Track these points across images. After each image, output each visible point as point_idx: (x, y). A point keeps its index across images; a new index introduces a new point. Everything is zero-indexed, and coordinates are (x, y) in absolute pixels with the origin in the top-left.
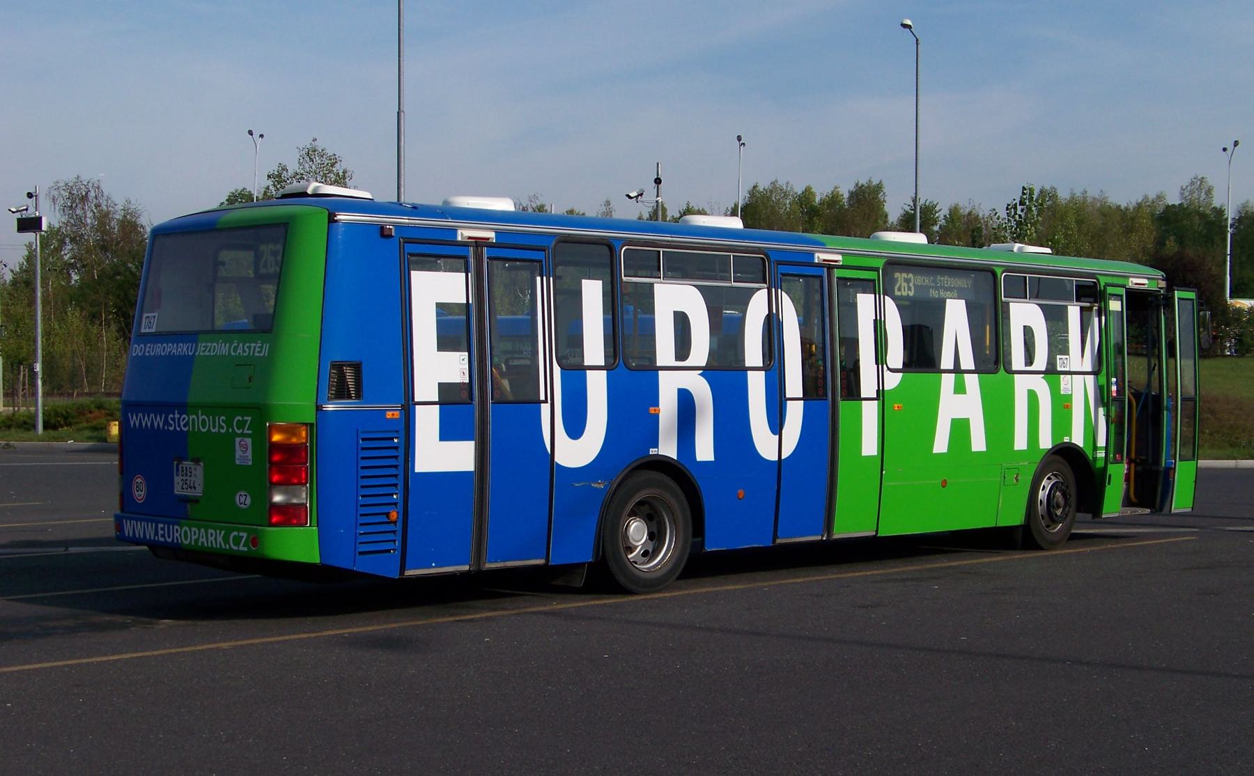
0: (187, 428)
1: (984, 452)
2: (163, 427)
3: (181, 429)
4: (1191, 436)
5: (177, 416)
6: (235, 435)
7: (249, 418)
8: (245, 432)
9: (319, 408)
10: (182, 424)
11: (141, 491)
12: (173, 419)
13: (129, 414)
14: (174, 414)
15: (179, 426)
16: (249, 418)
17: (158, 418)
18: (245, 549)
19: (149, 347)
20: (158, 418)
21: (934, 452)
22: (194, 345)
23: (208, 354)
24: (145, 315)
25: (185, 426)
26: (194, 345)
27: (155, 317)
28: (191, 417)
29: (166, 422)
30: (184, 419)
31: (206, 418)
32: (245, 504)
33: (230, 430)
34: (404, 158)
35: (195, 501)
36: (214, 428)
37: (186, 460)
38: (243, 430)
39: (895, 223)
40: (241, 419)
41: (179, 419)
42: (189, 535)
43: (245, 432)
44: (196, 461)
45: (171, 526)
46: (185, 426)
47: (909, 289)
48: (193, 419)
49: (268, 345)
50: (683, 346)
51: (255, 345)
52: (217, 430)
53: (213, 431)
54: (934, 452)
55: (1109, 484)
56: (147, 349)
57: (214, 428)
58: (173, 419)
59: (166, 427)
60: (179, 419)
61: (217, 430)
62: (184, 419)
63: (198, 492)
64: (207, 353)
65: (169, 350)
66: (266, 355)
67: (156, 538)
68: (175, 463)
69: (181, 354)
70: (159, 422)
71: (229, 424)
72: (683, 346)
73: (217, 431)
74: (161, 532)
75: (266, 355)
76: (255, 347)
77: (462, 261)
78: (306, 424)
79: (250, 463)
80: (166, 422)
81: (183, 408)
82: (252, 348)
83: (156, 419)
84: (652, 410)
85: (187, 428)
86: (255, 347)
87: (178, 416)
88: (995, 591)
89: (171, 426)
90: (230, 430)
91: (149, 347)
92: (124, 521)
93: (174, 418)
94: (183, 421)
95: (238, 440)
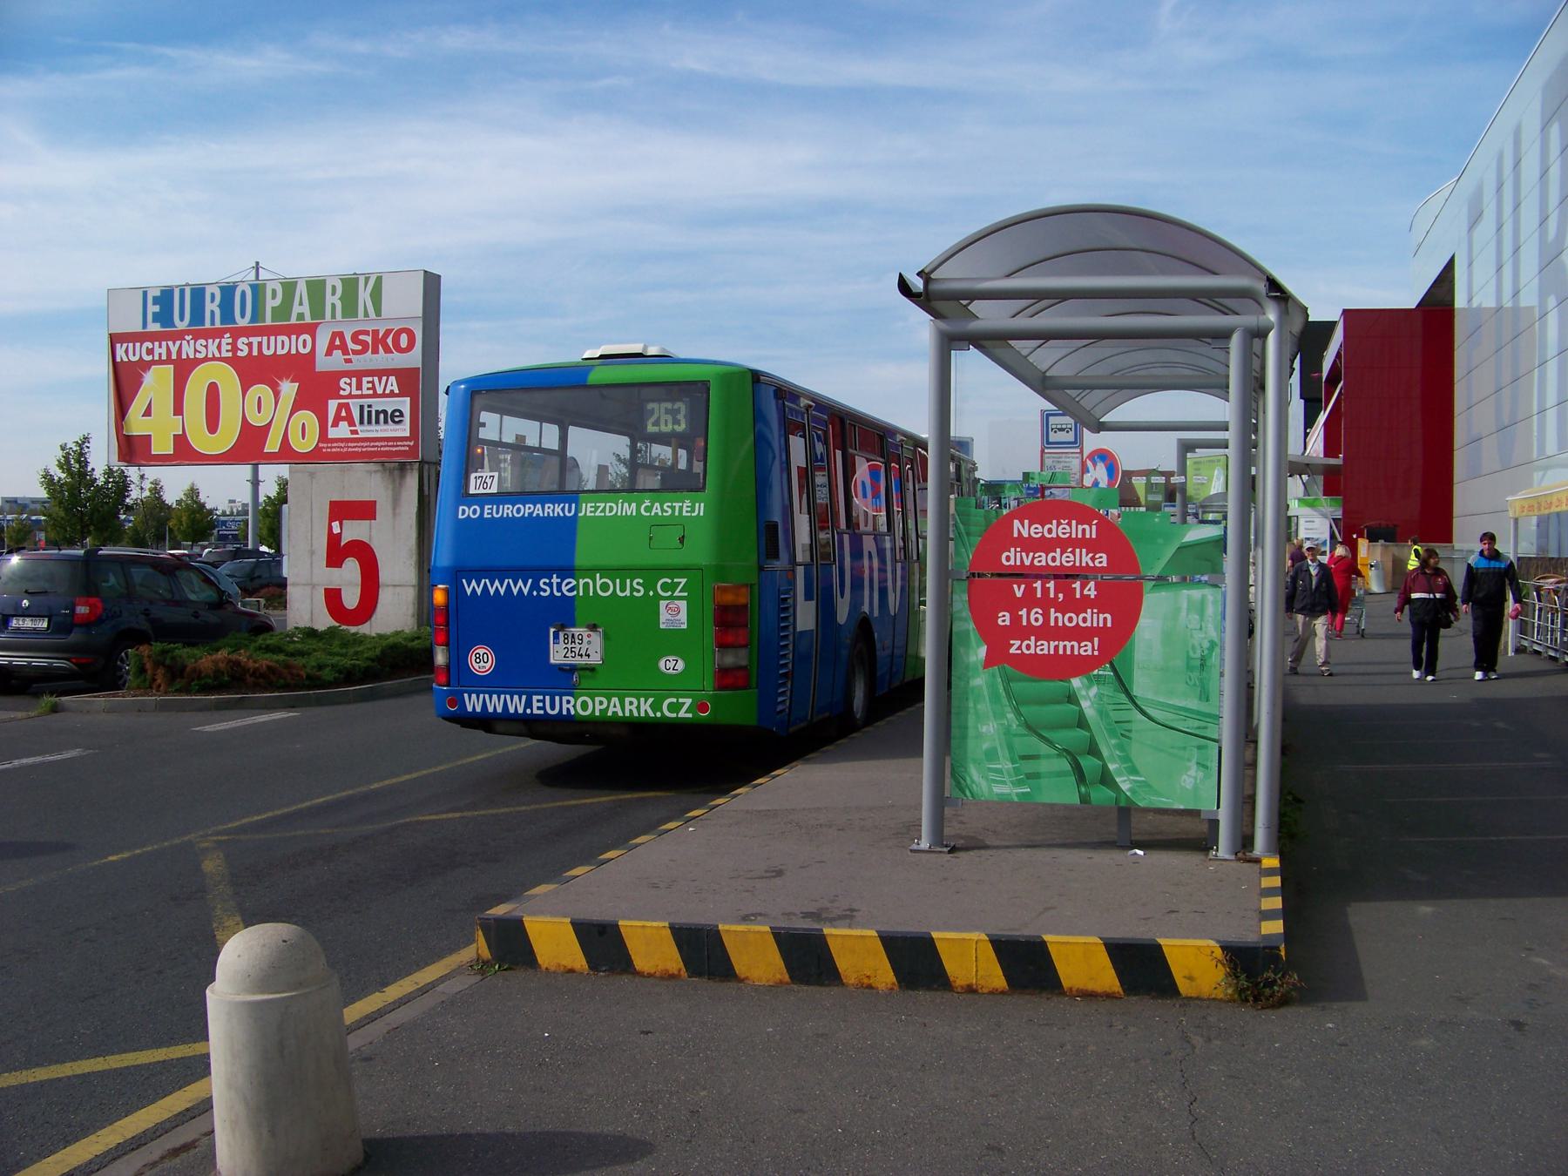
1: (327, 435)
2: (530, 592)
3: (563, 593)
4: (1506, 425)
5: (555, 580)
6: (658, 598)
7: (684, 581)
9: (761, 569)
10: (564, 589)
12: (550, 585)
15: (559, 589)
16: (684, 581)
17: (520, 583)
18: (690, 715)
20: (520, 583)
21: (265, 451)
22: (574, 505)
24: (473, 476)
26: (574, 505)
27: (493, 477)
28: (582, 582)
29: (535, 586)
33: (651, 593)
35: (591, 669)
36: (623, 590)
37: (574, 626)
38: (673, 593)
40: (670, 581)
41: (559, 585)
42: (583, 705)
44: (593, 627)
45: (557, 698)
48: (586, 585)
49: (702, 505)
50: (213, 300)
51: (681, 504)
52: (628, 593)
54: (265, 451)
56: (486, 511)
57: (623, 590)
58: (550, 585)
59: (535, 593)
60: (559, 585)
61: (628, 593)
63: (595, 659)
65: (527, 511)
66: (702, 514)
68: (552, 630)
70: (522, 587)
72: (213, 300)
73: (628, 595)
74: (535, 704)
75: (702, 514)
77: (1050, 440)
78: (747, 585)
79: (685, 627)
80: (535, 586)
81: (567, 571)
82: (677, 509)
86: (681, 508)
87: (559, 580)
88: (848, 913)
90: (651, 593)
92: (466, 695)
94: (566, 585)
95: (663, 603)
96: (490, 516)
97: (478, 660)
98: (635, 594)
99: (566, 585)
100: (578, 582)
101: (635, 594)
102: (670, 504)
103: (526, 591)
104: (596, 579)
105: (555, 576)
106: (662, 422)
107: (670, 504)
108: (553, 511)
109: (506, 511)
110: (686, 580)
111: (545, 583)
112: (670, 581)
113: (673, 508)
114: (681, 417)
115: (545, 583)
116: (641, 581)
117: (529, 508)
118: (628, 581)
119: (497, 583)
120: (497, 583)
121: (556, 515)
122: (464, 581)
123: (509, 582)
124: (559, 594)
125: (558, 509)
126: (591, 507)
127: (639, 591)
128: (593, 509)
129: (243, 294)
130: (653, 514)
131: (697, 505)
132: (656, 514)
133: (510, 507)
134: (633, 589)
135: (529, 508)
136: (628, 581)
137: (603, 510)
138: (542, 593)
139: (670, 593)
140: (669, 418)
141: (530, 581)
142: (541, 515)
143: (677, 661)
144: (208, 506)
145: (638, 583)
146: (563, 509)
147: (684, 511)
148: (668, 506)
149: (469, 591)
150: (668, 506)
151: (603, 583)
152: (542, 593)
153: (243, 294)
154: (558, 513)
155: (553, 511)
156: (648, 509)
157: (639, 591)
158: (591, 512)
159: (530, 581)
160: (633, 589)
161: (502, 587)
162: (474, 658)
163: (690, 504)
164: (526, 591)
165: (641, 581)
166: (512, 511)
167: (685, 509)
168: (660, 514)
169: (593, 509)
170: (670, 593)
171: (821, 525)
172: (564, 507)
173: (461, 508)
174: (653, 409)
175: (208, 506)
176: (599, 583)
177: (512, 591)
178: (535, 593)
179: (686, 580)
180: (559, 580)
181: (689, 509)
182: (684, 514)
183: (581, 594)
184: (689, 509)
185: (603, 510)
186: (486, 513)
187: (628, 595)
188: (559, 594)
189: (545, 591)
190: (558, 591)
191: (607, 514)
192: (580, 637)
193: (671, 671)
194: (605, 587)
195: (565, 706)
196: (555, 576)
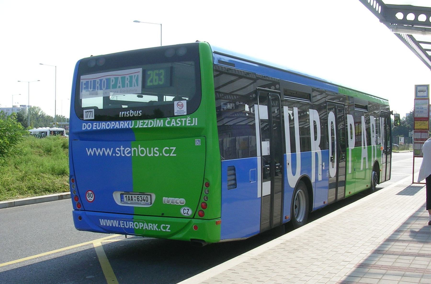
0: (130, 155)
2: (112, 154)
3: (125, 155)
5: (122, 149)
7: (174, 148)
8: (171, 155)
10: (126, 153)
11: (92, 197)
12: (120, 151)
13: (87, 149)
14: (120, 148)
15: (124, 153)
16: (174, 148)
17: (108, 150)
19: (96, 125)
20: (108, 150)
23: (147, 126)
25: (128, 154)
28: (133, 149)
29: (114, 152)
30: (128, 150)
31: (144, 150)
32: (187, 214)
33: (161, 154)
34: (315, 200)
36: (150, 154)
39: (97, 115)
40: (168, 148)
41: (124, 150)
43: (171, 155)
45: (128, 222)
46: (128, 154)
47: (160, 80)
48: (135, 150)
49: (196, 119)
51: (185, 119)
52: (152, 155)
53: (150, 155)
55: (82, 92)
56: (94, 126)
57: (150, 154)
58: (120, 151)
59: (114, 155)
60: (124, 150)
61: (152, 155)
62: (128, 150)
64: (144, 126)
65: (112, 126)
67: (119, 226)
69: (123, 127)
71: (160, 151)
73: (152, 155)
74: (121, 224)
76: (185, 121)
80: (114, 152)
83: (97, 151)
84: (217, 113)
85: (130, 155)
86: (185, 121)
87: (123, 149)
89: (118, 154)
90: (161, 154)
91: (96, 125)
93: (120, 150)
94: (127, 151)
96: (95, 129)
97: (89, 196)
98: (155, 155)
99: (127, 151)
100: (131, 150)
101: (155, 155)
102: (180, 119)
103: (110, 154)
104: (138, 147)
105: (122, 146)
106: (154, 80)
107: (180, 119)
108: (124, 125)
109: (103, 126)
110: (175, 148)
111: (118, 150)
112: (168, 148)
113: (181, 121)
114: (162, 77)
115: (118, 150)
116: (158, 149)
117: (113, 124)
118: (152, 148)
119: (99, 150)
120: (99, 150)
121: (125, 127)
122: (87, 149)
123: (104, 149)
124: (123, 155)
125: (126, 125)
126: (142, 123)
127: (157, 154)
128: (142, 124)
129: (104, 81)
130: (171, 125)
131: (194, 119)
132: (173, 125)
133: (105, 123)
134: (154, 153)
135: (113, 124)
136: (152, 148)
137: (147, 125)
138: (117, 155)
139: (168, 155)
140: (157, 78)
141: (112, 149)
142: (148, 229)
143: (189, 210)
144: (32, 107)
145: (156, 150)
146: (128, 124)
147: (187, 123)
148: (179, 121)
149: (89, 154)
150: (179, 121)
151: (142, 149)
152: (117, 155)
153: (104, 81)
154: (126, 126)
155: (124, 125)
156: (169, 123)
157: (157, 154)
158: (141, 125)
159: (112, 149)
160: (154, 153)
161: (101, 151)
162: (87, 195)
163: (190, 119)
164: (110, 154)
165: (158, 149)
166: (105, 126)
167: (188, 122)
168: (175, 125)
169: (142, 124)
170: (168, 155)
171: (98, 80)
172: (129, 122)
173: (83, 124)
174: (150, 74)
175: (32, 107)
176: (140, 150)
177: (105, 153)
178: (114, 155)
179: (175, 148)
180: (123, 149)
181: (190, 122)
182: (187, 125)
183: (133, 155)
184: (190, 122)
185: (147, 125)
186: (94, 127)
187: (152, 155)
188: (123, 155)
189: (118, 154)
190: (123, 154)
191: (149, 126)
192: (138, 200)
193: (186, 214)
194: (142, 152)
195: (130, 225)
196: (122, 146)
